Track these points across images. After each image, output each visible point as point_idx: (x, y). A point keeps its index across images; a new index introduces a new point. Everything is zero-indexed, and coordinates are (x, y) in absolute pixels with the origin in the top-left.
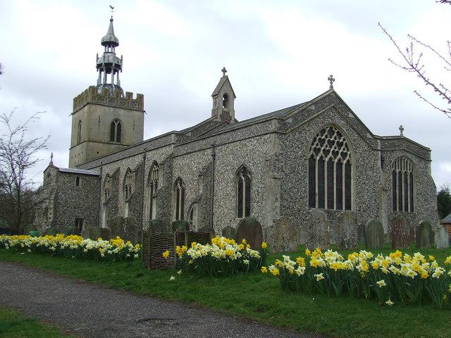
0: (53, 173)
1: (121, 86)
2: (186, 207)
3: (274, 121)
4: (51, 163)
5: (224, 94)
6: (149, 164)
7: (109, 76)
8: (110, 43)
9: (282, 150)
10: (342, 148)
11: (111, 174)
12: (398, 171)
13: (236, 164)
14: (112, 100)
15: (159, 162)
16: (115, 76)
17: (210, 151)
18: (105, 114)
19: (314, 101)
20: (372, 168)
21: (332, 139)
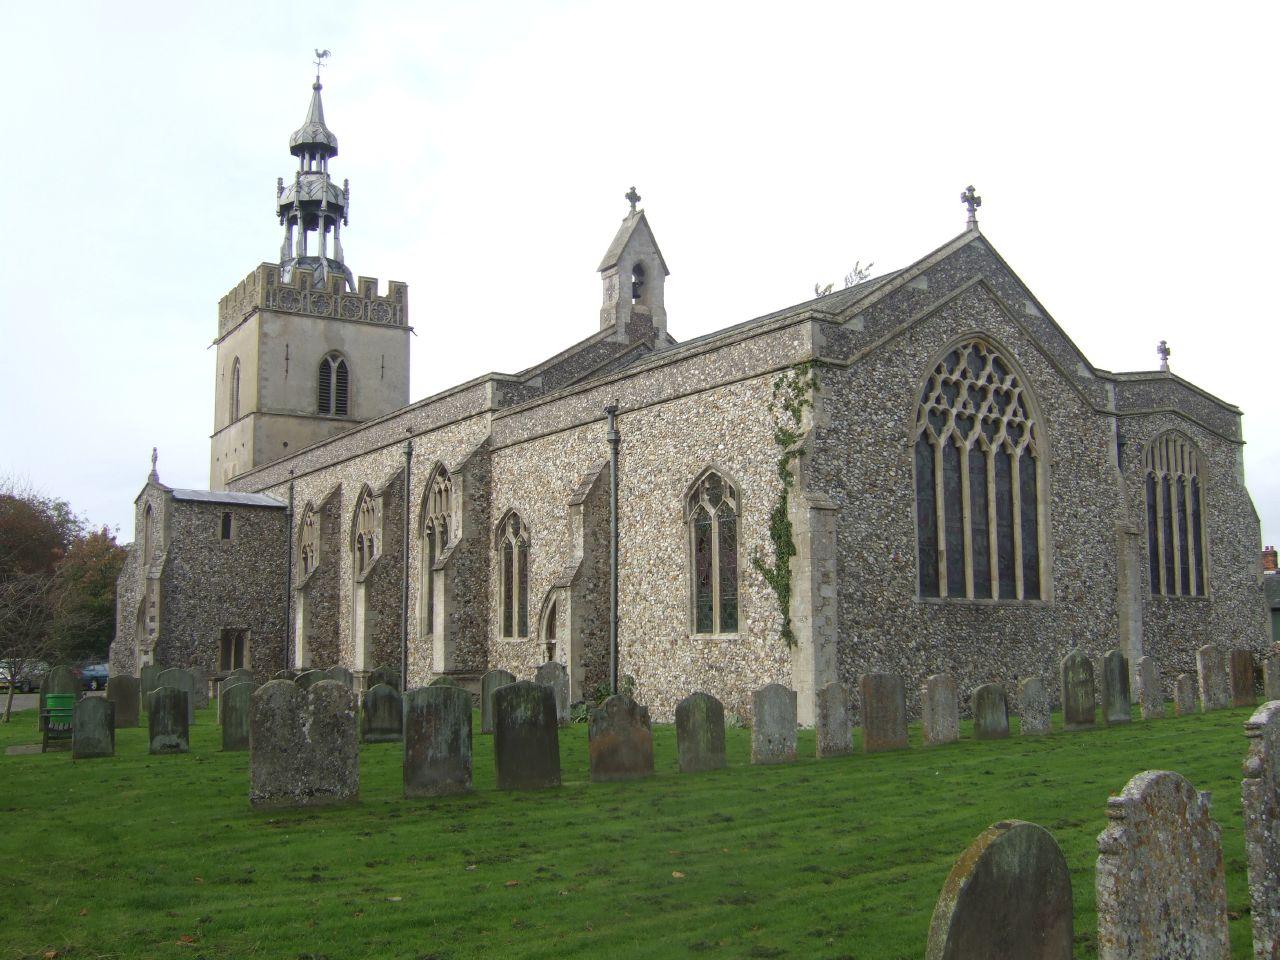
0: (158, 505)
1: (347, 263)
2: (535, 600)
3: (808, 325)
4: (154, 476)
5: (637, 266)
6: (421, 473)
7: (314, 237)
8: (316, 148)
9: (835, 417)
10: (1010, 410)
11: (318, 502)
12: (1160, 474)
13: (688, 467)
14: (320, 300)
15: (451, 465)
16: (330, 236)
17: (602, 430)
18: (311, 336)
19: (925, 266)
20: (1093, 470)
21: (981, 382)
